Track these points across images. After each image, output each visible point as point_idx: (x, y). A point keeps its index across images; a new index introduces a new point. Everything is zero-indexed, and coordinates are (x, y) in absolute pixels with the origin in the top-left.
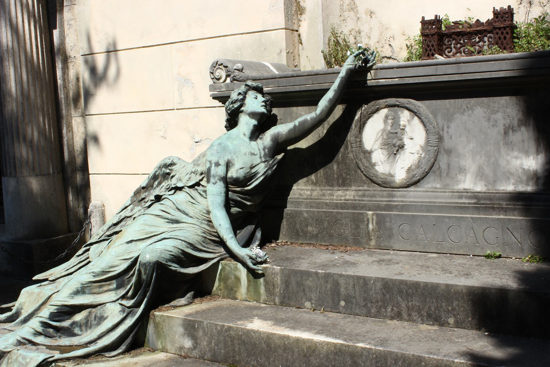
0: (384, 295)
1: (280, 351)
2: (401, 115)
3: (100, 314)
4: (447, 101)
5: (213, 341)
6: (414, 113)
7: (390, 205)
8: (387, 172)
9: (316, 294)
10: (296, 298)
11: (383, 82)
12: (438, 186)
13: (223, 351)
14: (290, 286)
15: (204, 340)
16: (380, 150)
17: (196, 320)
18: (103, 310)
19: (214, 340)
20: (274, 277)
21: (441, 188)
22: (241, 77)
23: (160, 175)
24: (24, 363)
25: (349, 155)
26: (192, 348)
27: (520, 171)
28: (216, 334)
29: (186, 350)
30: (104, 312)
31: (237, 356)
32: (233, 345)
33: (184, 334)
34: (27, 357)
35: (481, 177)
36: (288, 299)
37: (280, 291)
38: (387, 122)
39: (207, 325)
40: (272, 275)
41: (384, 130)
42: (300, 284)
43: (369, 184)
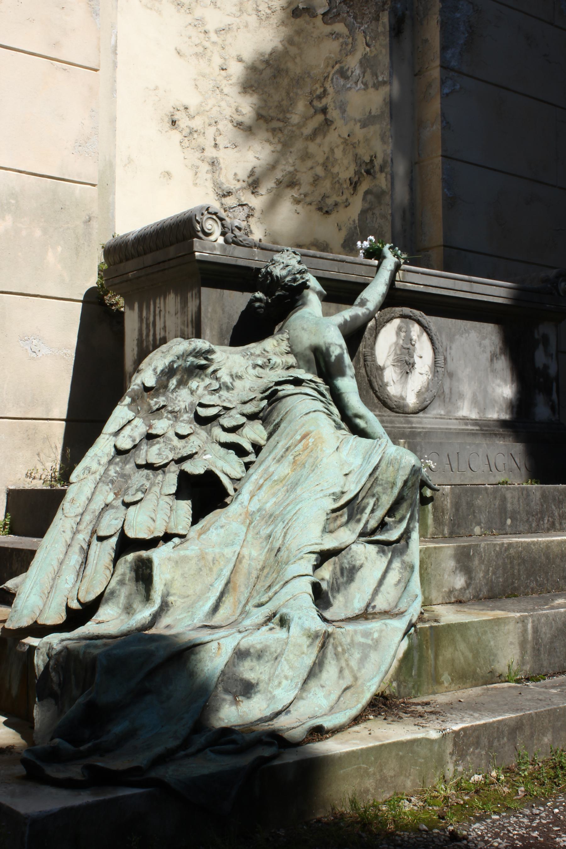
0: (542, 506)
1: (558, 560)
2: (412, 329)
3: (349, 563)
4: (450, 320)
5: (491, 569)
6: (425, 328)
7: (414, 431)
8: (398, 394)
9: (485, 515)
10: (466, 523)
11: (410, 286)
12: (443, 412)
13: (501, 580)
14: (460, 510)
15: (480, 571)
16: (392, 366)
17: (471, 545)
18: (352, 557)
19: (492, 567)
20: (444, 500)
21: (445, 415)
22: (244, 240)
23: (180, 368)
24: (370, 642)
25: (361, 371)
26: (464, 588)
27: (501, 399)
28: (494, 558)
29: (456, 593)
30: (353, 559)
31: (516, 581)
32: (512, 567)
33: (456, 568)
34: (372, 631)
35: (475, 404)
36: (458, 528)
37: (450, 518)
38: (400, 334)
39: (484, 548)
40: (442, 497)
41: (396, 344)
42: (470, 505)
43: (380, 408)
